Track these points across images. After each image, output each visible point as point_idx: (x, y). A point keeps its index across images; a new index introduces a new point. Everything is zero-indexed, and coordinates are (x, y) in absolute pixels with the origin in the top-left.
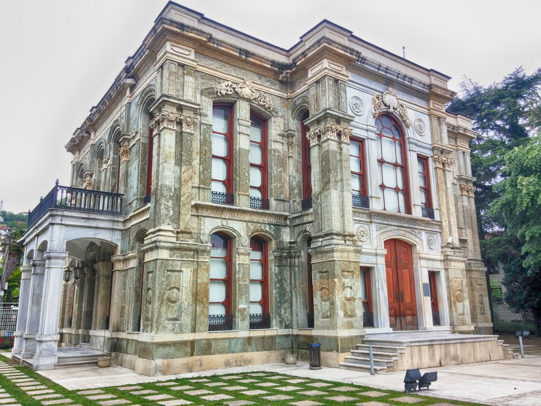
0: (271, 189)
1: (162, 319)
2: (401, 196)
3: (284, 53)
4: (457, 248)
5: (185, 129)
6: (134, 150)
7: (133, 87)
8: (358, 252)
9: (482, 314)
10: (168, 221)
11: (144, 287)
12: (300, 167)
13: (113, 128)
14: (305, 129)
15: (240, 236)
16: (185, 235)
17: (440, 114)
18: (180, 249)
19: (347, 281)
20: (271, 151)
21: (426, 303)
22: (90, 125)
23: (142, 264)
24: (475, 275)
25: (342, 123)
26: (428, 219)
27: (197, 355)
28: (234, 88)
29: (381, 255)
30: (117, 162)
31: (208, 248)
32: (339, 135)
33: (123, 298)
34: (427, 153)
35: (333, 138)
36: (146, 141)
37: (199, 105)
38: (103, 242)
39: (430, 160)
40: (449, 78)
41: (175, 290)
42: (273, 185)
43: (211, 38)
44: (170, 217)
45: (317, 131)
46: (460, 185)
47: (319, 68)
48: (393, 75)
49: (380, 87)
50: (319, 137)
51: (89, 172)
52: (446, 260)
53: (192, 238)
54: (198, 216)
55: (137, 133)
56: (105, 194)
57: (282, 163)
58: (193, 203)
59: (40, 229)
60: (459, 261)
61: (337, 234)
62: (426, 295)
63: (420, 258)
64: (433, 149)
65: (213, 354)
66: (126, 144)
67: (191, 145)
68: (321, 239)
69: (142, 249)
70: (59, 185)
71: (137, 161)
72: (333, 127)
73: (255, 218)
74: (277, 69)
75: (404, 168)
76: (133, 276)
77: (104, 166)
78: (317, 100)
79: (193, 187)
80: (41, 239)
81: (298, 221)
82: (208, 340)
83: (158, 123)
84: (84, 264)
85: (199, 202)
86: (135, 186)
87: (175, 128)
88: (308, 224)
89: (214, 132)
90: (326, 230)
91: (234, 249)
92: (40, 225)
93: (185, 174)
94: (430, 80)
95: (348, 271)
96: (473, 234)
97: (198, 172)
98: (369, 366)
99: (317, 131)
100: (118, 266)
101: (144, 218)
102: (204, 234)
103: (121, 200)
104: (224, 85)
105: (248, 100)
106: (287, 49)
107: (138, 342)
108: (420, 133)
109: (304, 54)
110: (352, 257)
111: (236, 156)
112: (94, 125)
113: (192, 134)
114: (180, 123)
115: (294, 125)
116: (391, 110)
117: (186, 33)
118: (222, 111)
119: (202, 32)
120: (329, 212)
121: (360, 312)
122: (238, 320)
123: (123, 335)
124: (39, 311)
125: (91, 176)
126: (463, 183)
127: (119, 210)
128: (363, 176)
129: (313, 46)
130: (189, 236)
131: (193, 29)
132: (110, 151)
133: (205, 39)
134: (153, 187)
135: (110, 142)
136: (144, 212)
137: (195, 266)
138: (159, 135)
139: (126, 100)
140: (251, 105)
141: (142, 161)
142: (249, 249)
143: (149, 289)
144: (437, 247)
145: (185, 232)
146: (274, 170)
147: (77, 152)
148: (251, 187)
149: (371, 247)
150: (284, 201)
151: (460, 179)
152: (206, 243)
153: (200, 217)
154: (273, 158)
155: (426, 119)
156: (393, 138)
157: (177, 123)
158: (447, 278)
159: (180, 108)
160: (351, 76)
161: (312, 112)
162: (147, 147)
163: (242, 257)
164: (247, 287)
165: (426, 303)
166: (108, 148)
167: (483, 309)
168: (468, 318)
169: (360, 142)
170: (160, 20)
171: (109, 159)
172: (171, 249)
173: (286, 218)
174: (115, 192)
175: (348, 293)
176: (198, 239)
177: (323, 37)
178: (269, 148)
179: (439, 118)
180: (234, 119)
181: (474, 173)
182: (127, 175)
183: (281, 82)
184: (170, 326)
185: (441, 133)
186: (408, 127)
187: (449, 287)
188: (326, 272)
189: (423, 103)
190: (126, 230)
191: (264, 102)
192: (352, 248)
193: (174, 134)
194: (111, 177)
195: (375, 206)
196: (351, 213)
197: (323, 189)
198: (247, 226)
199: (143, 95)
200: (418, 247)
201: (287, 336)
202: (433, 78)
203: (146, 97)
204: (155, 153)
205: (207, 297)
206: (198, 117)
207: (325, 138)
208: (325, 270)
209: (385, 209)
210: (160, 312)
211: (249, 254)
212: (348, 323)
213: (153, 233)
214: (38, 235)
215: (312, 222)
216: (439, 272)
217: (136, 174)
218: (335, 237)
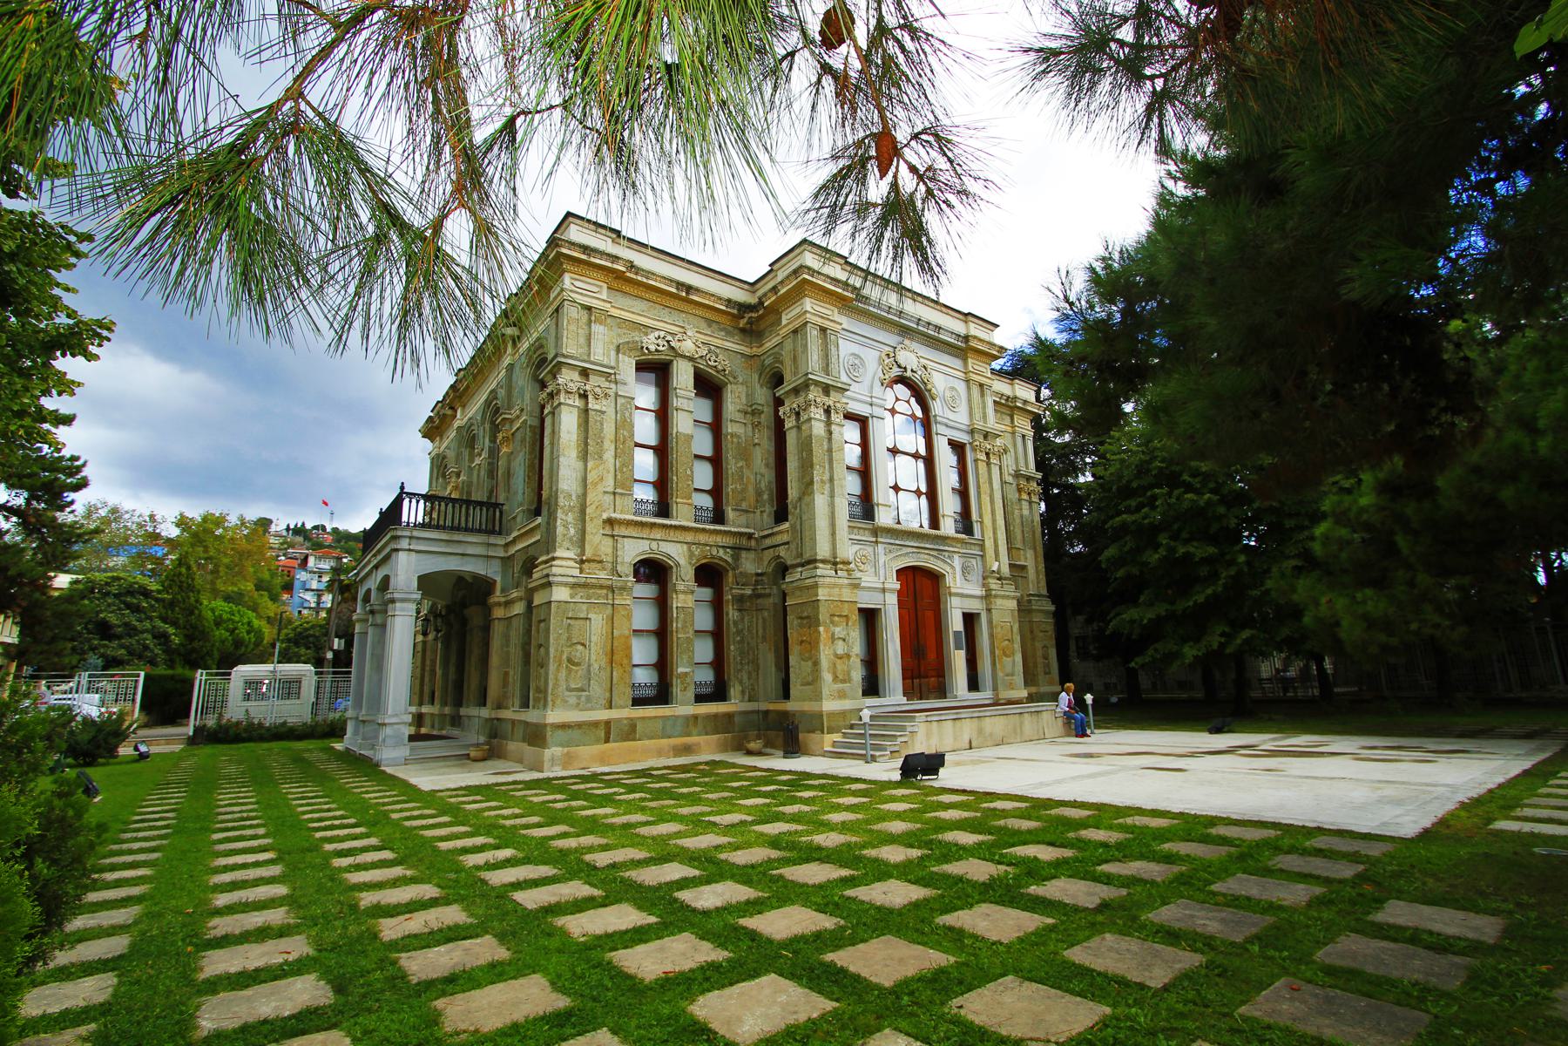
0: (728, 494)
1: (560, 689)
3: (746, 287)
4: (1006, 579)
5: (592, 404)
6: (519, 436)
7: (515, 341)
8: (856, 586)
9: (1046, 673)
10: (566, 544)
11: (534, 643)
12: (772, 460)
13: (488, 403)
14: (779, 402)
15: (678, 565)
16: (594, 565)
17: (983, 380)
18: (585, 586)
19: (838, 631)
21: (959, 659)
22: (454, 398)
23: (530, 607)
24: (1037, 618)
25: (832, 393)
26: (963, 536)
27: (615, 741)
28: (668, 342)
29: (891, 591)
30: (494, 453)
31: (629, 584)
32: (828, 411)
33: (506, 661)
34: (963, 438)
35: (818, 416)
36: (536, 423)
37: (612, 368)
38: (476, 577)
39: (968, 448)
40: (997, 326)
41: (580, 647)
42: (730, 488)
43: (631, 266)
44: (571, 539)
45: (795, 406)
46: (1018, 485)
47: (798, 310)
48: (910, 321)
49: (891, 339)
50: (798, 414)
52: (988, 597)
53: (604, 569)
54: (613, 536)
55: (522, 410)
56: (481, 504)
57: (745, 454)
58: (605, 516)
59: (379, 557)
60: (1007, 597)
61: (823, 561)
62: (958, 647)
63: (950, 594)
64: (972, 432)
66: (507, 427)
67: (602, 429)
68: (800, 569)
69: (530, 586)
71: (522, 454)
72: (818, 400)
73: (702, 538)
74: (735, 311)
75: (929, 461)
76: (518, 625)
77: (477, 461)
78: (795, 359)
79: (605, 492)
80: (380, 574)
81: (768, 542)
82: (631, 719)
83: (551, 396)
84: (449, 609)
85: (613, 515)
86: (520, 492)
87: (577, 403)
89: (637, 408)
90: (807, 556)
91: (669, 585)
92: (379, 551)
93: (593, 473)
94: (968, 328)
95: (839, 616)
96: (1036, 557)
97: (612, 470)
98: (864, 752)
99: (795, 406)
100: (498, 613)
101: (533, 540)
102: (622, 563)
103: (501, 513)
104: (652, 337)
105: (691, 359)
106: (752, 280)
107: (526, 723)
108: (952, 408)
109: (774, 289)
110: (847, 595)
111: (673, 443)
112: (460, 397)
113: (603, 412)
114: (584, 396)
115: (762, 395)
116: (909, 374)
117: (592, 260)
118: (652, 376)
119: (615, 258)
120: (813, 528)
121: (858, 674)
122: (677, 689)
123: (506, 714)
124: (380, 680)
125: (458, 475)
126: (1023, 482)
127: (497, 528)
128: (865, 472)
129: (787, 277)
130: (599, 566)
131: (602, 254)
133: (624, 269)
134: (545, 494)
136: (532, 530)
137: (609, 610)
138: (553, 413)
139: (507, 361)
140: (695, 368)
141: (530, 453)
142: (692, 583)
143: (540, 646)
144: (976, 576)
145: (594, 561)
146: (731, 464)
148: (696, 490)
149: (876, 579)
150: (747, 511)
151: (1017, 475)
152: (627, 576)
154: (729, 446)
155: (961, 387)
157: (580, 395)
158: (990, 622)
159: (585, 373)
160: (845, 322)
161: (787, 377)
162: (538, 431)
163: (681, 597)
164: (689, 641)
165: (959, 659)
166: (481, 434)
167: (1048, 666)
168: (1019, 678)
169: (863, 422)
170: (553, 242)
172: (574, 586)
173: (750, 536)
174: (493, 501)
175: (840, 648)
176: (615, 571)
177: (801, 267)
178: (724, 431)
179: (981, 385)
181: (1038, 469)
182: (509, 474)
183: (743, 331)
184: (573, 701)
187: (991, 636)
188: (808, 617)
189: (957, 363)
190: (509, 558)
192: (846, 581)
193: (575, 411)
195: (884, 518)
196: (846, 529)
197: (804, 494)
198: (690, 550)
200: (949, 580)
201: (758, 712)
202: (972, 325)
204: (547, 441)
205: (629, 656)
206: (613, 386)
207: (806, 417)
208: (805, 614)
209: (899, 523)
210: (556, 679)
211: (693, 592)
212: (839, 692)
213: (546, 562)
214: (376, 567)
215: (787, 543)
216: (979, 614)
217: (522, 473)
218: (821, 565)
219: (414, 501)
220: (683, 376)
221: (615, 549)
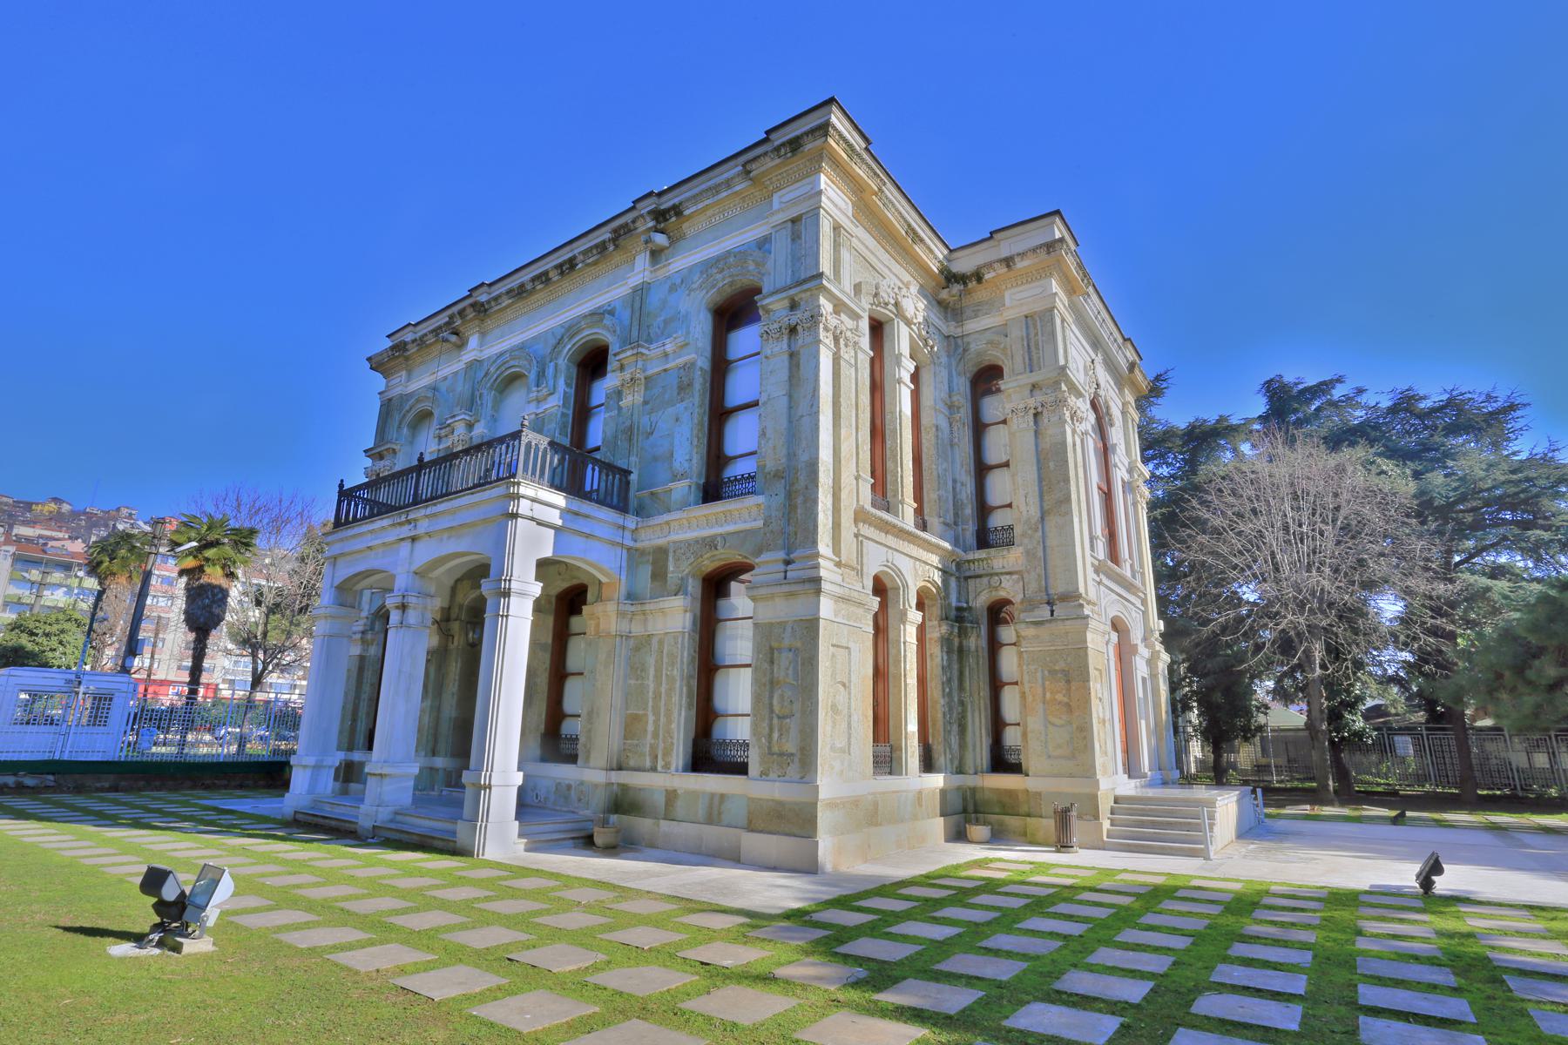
15: (906, 586)
51: (467, 418)
65: (880, 825)
88: (1008, 577)
132: (555, 376)
135: (556, 359)
147: (404, 373)
153: (860, 538)
186: (1111, 425)
221: (860, 553)
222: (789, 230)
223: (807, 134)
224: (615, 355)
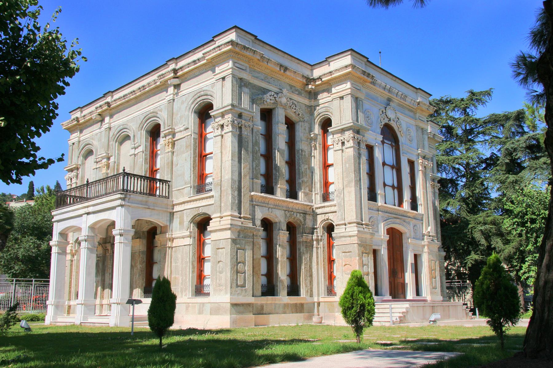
2: (396, 191)
20: (299, 151)
28: (275, 98)
70: (125, 171)
141: (194, 154)
156: (391, 145)
171: (140, 146)
180: (273, 123)
185: (423, 141)
191: (295, 109)
194: (144, 162)
198: (286, 215)
199: (196, 97)
203: (199, 100)
219: (133, 178)
220: (279, 117)
222: (221, 82)
223: (224, 44)
224: (162, 132)
